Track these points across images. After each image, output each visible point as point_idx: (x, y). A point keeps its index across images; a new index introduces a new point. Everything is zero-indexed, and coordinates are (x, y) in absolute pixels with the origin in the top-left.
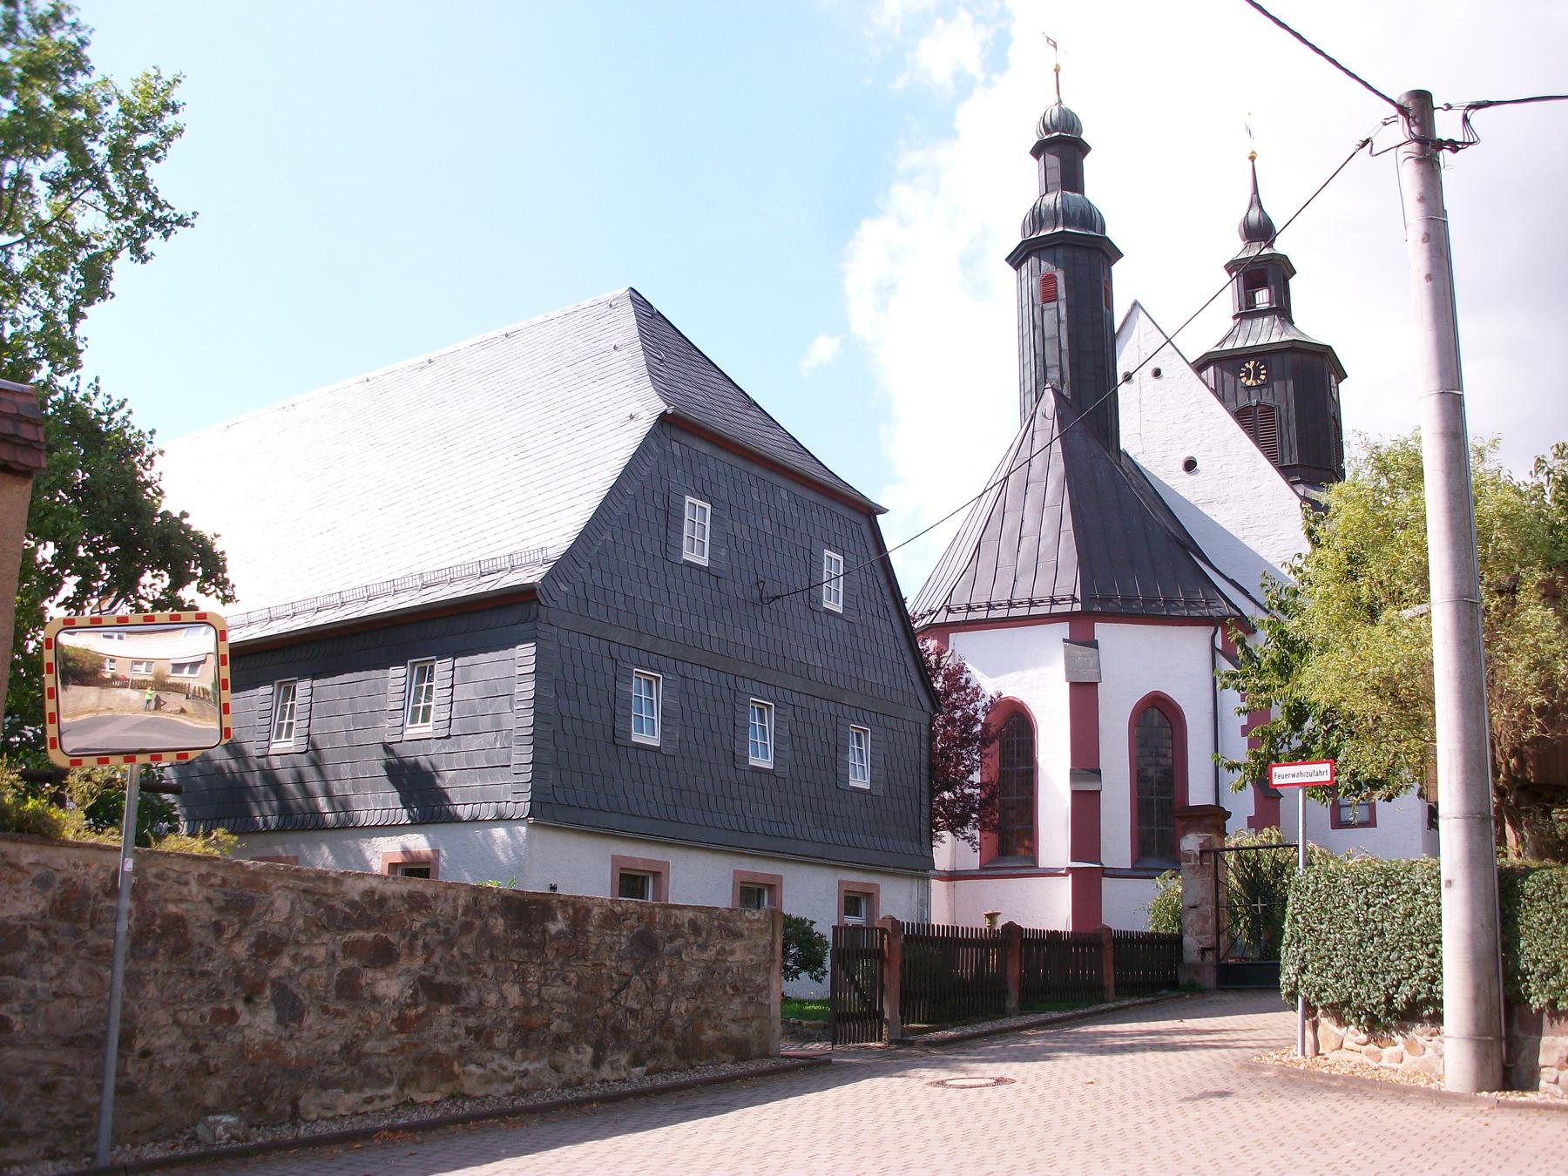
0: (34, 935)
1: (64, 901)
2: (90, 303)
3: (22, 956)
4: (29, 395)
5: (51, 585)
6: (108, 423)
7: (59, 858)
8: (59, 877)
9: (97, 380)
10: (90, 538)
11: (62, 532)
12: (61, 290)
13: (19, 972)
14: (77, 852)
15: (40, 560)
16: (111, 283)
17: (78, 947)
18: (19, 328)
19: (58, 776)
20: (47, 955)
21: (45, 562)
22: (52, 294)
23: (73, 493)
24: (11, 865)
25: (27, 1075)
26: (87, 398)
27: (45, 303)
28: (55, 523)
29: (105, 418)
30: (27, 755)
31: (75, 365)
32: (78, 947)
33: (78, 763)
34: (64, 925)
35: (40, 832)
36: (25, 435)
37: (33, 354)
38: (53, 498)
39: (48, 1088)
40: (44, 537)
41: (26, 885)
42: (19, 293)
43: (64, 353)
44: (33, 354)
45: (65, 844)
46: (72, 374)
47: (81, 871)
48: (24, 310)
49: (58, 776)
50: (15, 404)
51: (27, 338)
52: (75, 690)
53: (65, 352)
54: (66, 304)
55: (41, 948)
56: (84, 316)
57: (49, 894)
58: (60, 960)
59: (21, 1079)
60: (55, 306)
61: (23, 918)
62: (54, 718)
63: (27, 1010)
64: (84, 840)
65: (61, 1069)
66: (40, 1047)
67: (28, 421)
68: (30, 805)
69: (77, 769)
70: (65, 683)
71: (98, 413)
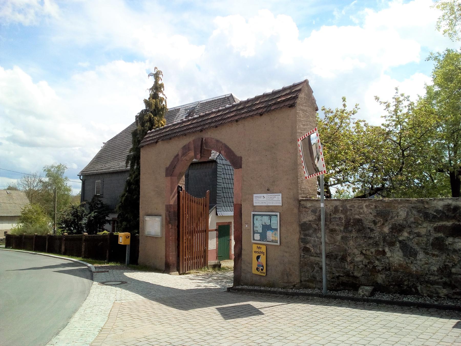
3: (311, 231)
41: (310, 212)
61: (310, 221)
63: (314, 246)
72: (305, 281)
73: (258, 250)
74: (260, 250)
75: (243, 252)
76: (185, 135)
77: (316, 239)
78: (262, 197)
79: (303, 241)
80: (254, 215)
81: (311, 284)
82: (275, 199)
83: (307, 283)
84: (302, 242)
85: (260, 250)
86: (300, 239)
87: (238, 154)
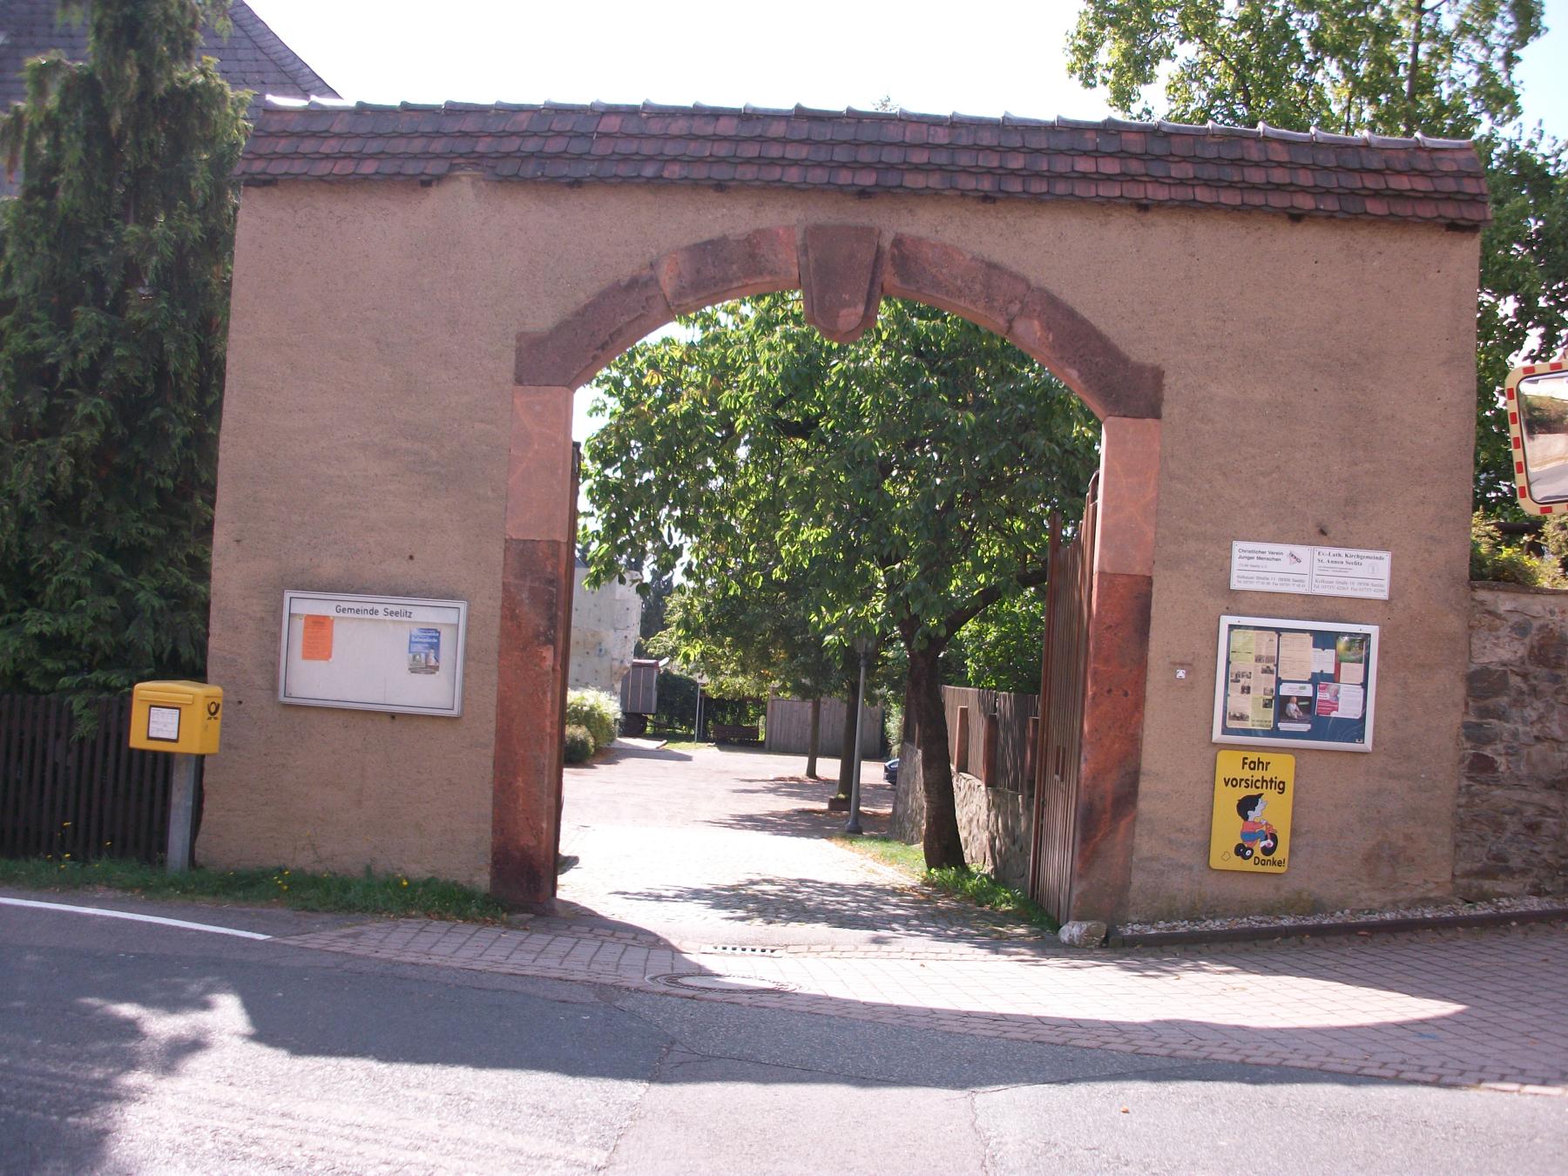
0: (1515, 680)
1: (1541, 647)
2: (1524, 44)
3: (1504, 700)
4: (1468, 149)
5: (1515, 339)
6: (1556, 166)
7: (1535, 605)
8: (1536, 624)
9: (1540, 123)
10: (1549, 287)
11: (1520, 285)
12: (1493, 39)
13: (1502, 716)
14: (1552, 599)
15: (1501, 315)
16: (1543, 19)
17: (1557, 692)
18: (1456, 86)
19: (1535, 526)
20: (1527, 699)
21: (1507, 317)
22: (1485, 44)
23: (1528, 244)
24: (1490, 613)
25: (1512, 814)
26: (1531, 144)
27: (1479, 55)
28: (1512, 277)
29: (1552, 161)
30: (1504, 509)
31: (1516, 111)
32: (1557, 692)
33: (1549, 510)
34: (1542, 671)
35: (1516, 580)
36: (1469, 190)
37: (1472, 109)
38: (1507, 251)
39: (1533, 827)
40: (1502, 292)
41: (1504, 631)
42: (1451, 51)
43: (1502, 102)
44: (1472, 109)
45: (1541, 591)
46: (1515, 122)
47: (1557, 618)
48: (1459, 68)
49: (1535, 526)
50: (1454, 160)
51: (1464, 95)
52: (1543, 440)
53: (1501, 99)
54: (1500, 52)
55: (1521, 693)
56: (1518, 59)
57: (1527, 640)
58: (1539, 705)
59: (1507, 817)
60: (1488, 57)
61: (1504, 664)
62: (1522, 467)
63: (1511, 752)
64: (1560, 587)
65: (1544, 810)
66: (1524, 787)
67: (1469, 175)
68: (1504, 555)
69: (1549, 516)
70: (1531, 432)
71: (1546, 157)
72: (1467, 874)
73: (1247, 774)
74: (1258, 774)
75: (1144, 786)
76: (720, 187)
77: (1521, 728)
78: (1285, 559)
79: (1474, 734)
80: (1232, 627)
81: (1488, 885)
82: (1357, 571)
83: (1475, 883)
84: (1468, 738)
85: (1258, 774)
86: (1466, 726)
87: (1139, 353)
